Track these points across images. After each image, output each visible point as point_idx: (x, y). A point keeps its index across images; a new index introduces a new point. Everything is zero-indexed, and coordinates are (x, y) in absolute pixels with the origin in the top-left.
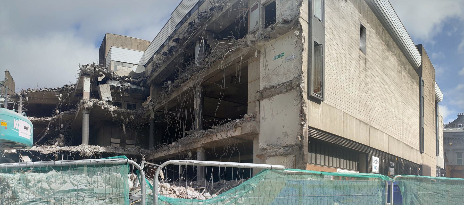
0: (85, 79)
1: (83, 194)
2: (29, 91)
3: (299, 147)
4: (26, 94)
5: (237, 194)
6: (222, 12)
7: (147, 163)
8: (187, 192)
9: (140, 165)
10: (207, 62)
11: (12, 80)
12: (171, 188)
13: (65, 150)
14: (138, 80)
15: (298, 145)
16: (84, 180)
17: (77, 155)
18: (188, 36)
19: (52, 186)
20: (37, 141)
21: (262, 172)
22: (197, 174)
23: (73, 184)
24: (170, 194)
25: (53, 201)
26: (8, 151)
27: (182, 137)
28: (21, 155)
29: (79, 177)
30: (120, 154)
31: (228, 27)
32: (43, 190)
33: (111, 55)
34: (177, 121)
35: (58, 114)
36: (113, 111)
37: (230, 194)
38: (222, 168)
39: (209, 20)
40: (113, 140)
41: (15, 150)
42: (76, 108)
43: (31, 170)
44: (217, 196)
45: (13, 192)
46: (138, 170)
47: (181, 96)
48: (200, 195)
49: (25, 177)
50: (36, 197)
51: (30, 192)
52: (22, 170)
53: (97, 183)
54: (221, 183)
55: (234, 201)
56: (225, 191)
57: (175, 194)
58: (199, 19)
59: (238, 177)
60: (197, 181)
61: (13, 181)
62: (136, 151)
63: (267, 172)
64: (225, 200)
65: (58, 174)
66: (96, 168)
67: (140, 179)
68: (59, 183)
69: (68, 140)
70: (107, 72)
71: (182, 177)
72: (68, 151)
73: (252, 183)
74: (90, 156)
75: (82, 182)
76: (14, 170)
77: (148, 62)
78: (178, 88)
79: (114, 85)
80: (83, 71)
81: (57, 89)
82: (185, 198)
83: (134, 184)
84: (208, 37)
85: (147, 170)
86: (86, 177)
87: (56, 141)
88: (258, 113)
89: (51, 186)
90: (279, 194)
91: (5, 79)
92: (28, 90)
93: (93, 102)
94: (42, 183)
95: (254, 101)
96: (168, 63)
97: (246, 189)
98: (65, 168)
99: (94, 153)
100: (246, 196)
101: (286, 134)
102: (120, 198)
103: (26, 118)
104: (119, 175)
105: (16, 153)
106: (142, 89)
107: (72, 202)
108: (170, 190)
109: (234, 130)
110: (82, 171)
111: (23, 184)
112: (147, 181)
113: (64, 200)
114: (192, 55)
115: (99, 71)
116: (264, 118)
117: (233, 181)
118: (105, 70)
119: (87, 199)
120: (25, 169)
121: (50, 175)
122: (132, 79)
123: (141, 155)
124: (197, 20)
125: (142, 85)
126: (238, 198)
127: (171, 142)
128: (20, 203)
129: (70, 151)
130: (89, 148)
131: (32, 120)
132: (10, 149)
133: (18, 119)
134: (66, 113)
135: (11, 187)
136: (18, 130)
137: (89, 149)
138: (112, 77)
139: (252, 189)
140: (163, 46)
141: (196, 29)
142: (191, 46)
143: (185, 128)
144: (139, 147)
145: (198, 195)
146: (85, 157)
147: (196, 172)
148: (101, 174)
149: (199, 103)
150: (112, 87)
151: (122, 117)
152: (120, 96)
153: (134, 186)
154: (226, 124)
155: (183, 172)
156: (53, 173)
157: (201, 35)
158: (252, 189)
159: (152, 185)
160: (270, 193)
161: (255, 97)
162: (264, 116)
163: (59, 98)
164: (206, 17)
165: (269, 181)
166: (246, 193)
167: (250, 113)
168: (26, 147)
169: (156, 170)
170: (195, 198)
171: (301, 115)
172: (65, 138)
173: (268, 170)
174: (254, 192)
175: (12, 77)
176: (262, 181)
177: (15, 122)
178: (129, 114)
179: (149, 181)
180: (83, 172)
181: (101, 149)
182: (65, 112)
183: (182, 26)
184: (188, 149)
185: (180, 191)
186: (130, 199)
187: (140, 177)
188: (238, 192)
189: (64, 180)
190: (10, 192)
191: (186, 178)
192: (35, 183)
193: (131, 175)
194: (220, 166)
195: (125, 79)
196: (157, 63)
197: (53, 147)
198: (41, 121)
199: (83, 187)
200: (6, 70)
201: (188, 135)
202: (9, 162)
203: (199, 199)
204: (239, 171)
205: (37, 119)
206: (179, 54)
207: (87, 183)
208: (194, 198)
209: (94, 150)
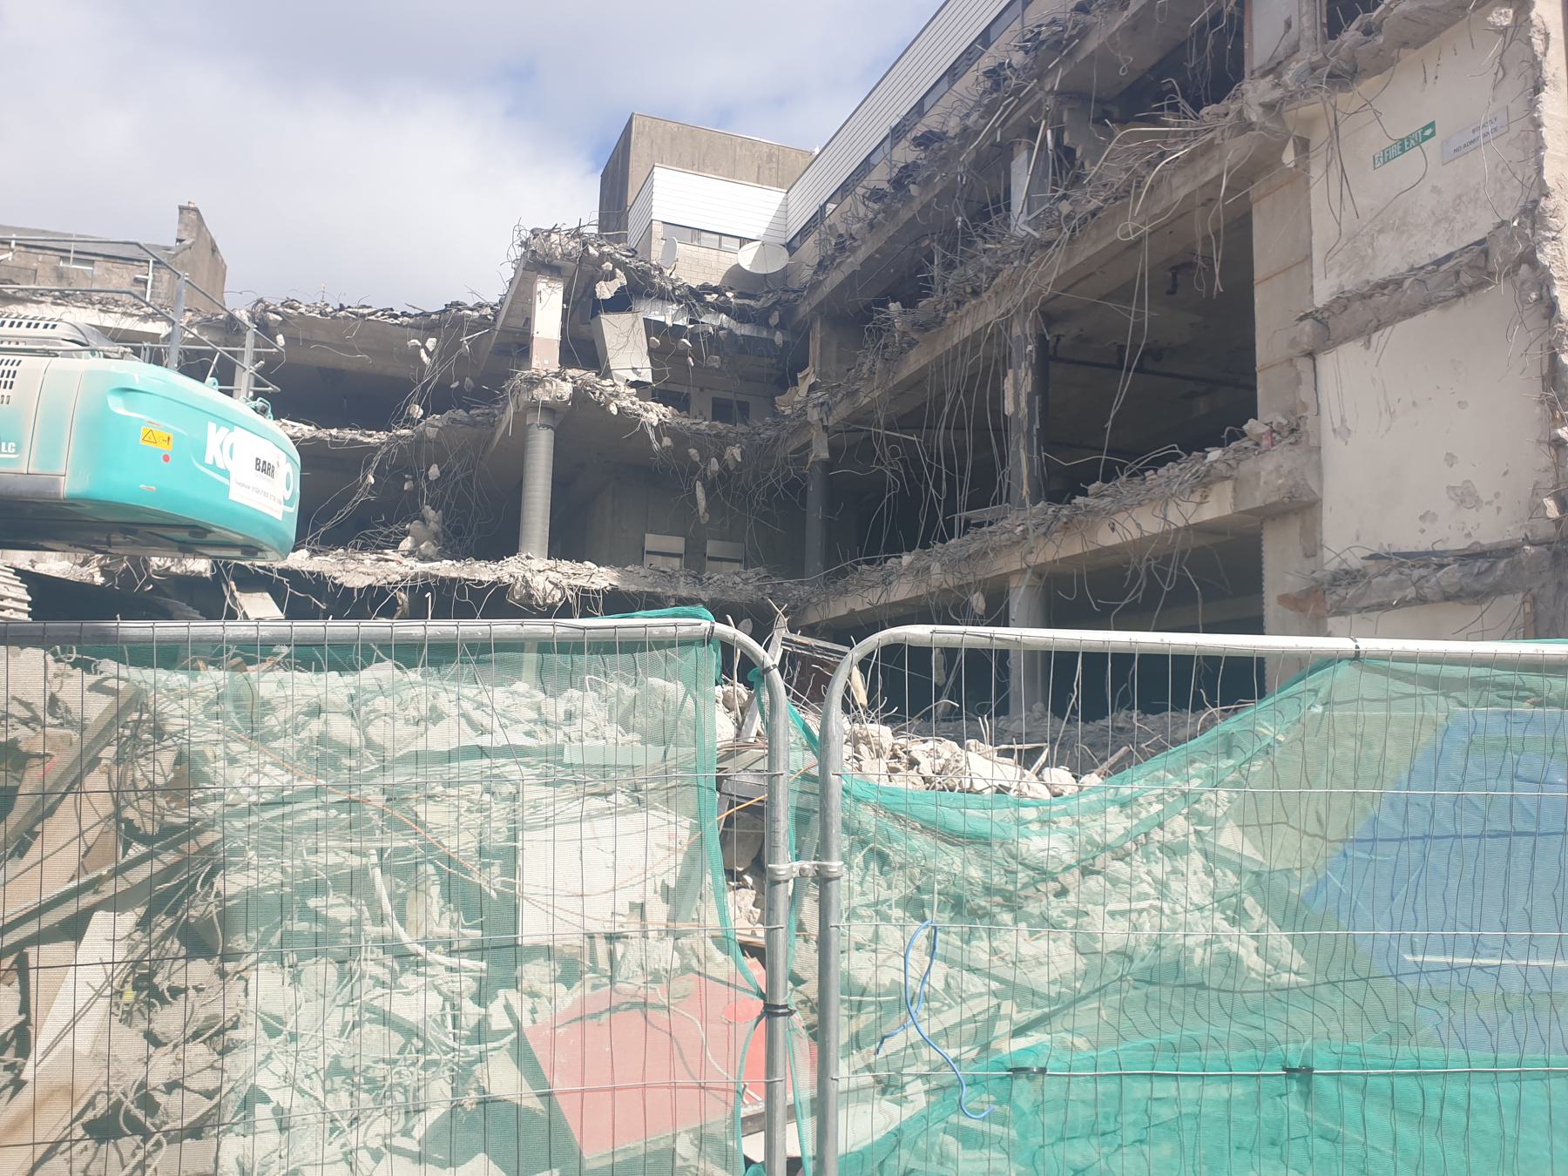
0: (542, 285)
1: (517, 768)
2: (290, 311)
3: (1550, 554)
4: (276, 320)
5: (1193, 777)
6: (1126, 13)
7: (795, 637)
8: (967, 762)
9: (766, 649)
10: (1069, 217)
11: (214, 250)
12: (897, 747)
13: (441, 574)
14: (760, 303)
15: (1547, 543)
16: (524, 710)
17: (498, 602)
18: (982, 122)
19: (377, 732)
20: (316, 528)
21: (1311, 672)
22: (1012, 685)
23: (472, 724)
24: (895, 770)
25: (378, 800)
26: (168, 564)
27: (951, 537)
28: (234, 588)
29: (500, 695)
30: (681, 601)
31: (1152, 69)
32: (329, 751)
33: (652, 186)
34: (930, 467)
35: (419, 422)
36: (655, 424)
37: (1162, 772)
38: (1123, 659)
39: (1070, 54)
40: (652, 541)
41: (204, 561)
42: (496, 402)
43: (279, 658)
44: (1100, 780)
45: (179, 760)
46: (758, 669)
47: (947, 364)
48: (1023, 775)
49: (245, 691)
50: (295, 783)
51: (268, 759)
52: (235, 655)
53: (578, 721)
54: (1120, 725)
55: (1180, 805)
56: (1139, 762)
57: (913, 772)
58: (1027, 53)
59: (1197, 695)
60: (1011, 712)
61: (187, 707)
62: (750, 587)
63: (1338, 675)
64: (1141, 800)
65: (406, 680)
66: (576, 657)
67: (766, 708)
68: (407, 721)
69: (457, 532)
70: (633, 263)
71: (944, 701)
72: (455, 579)
73: (1265, 724)
74: (553, 606)
75: (516, 715)
76: (193, 654)
77: (804, 232)
78: (934, 330)
79: (661, 319)
80: (534, 252)
81: (416, 315)
82: (958, 788)
83: (739, 728)
84: (1065, 118)
85: (794, 669)
86: (532, 696)
87: (406, 534)
88: (1313, 410)
89: (371, 730)
90: (1404, 776)
91: (179, 241)
92: (289, 304)
93: (575, 382)
94: (330, 716)
95: (1290, 360)
96: (890, 229)
97: (1237, 752)
98: (441, 654)
99: (569, 592)
100: (1236, 784)
101: (1465, 497)
102: (679, 790)
103: (269, 423)
104: (675, 689)
105: (208, 574)
106: (779, 338)
107: (465, 804)
108: (895, 756)
109: (1197, 497)
110: (516, 670)
111: (237, 723)
112: (795, 715)
113: (430, 797)
114: (998, 196)
115: (603, 257)
116: (1343, 432)
117: (1174, 714)
118: (627, 256)
119: (534, 792)
120: (252, 652)
121: (368, 682)
122: (735, 297)
123: (769, 604)
124: (1018, 58)
125: (777, 321)
126: (1201, 794)
127: (895, 549)
128: (210, 813)
129: (466, 580)
130: (550, 573)
131: (299, 435)
132: (181, 555)
133: (229, 422)
134: (454, 421)
135: (172, 735)
136: (225, 473)
137: (552, 575)
138: (653, 285)
139: (1267, 751)
140: (866, 166)
141: (1019, 89)
142: (996, 160)
143: (963, 497)
144: (762, 571)
145: (1018, 779)
146: (529, 608)
147: (1008, 676)
148: (599, 683)
149: (1029, 389)
150: (653, 328)
151: (693, 451)
152: (688, 364)
153: (738, 735)
154: (1156, 471)
155: (948, 678)
156: (382, 672)
157: (1037, 110)
158: (1268, 753)
159: (817, 733)
160: (1356, 771)
161: (1293, 343)
162: (1343, 420)
163: (422, 351)
164: (1059, 42)
165: (1348, 713)
166: (1237, 768)
167: (1268, 413)
168: (262, 551)
169: (833, 670)
170: (1002, 790)
171: (1553, 394)
172: (444, 523)
173: (1339, 661)
174: (1274, 768)
175: (212, 241)
176: (1314, 716)
177: (215, 437)
178: (722, 442)
179: (802, 715)
180: (520, 672)
181: (602, 578)
182: (449, 413)
183: (954, 87)
184: (970, 579)
185: (937, 761)
186: (721, 793)
187: (766, 698)
188: (1201, 767)
189: (433, 709)
190: (167, 759)
191: (961, 704)
192: (294, 717)
193: (727, 688)
194: (1113, 648)
195: (709, 298)
196: (841, 231)
197: (387, 560)
198: (341, 444)
199: (518, 739)
200: (186, 205)
201: (980, 525)
202: (167, 615)
203: (1021, 794)
204: (1198, 672)
205: (322, 434)
206: (937, 191)
207: (535, 722)
208: (998, 791)
209: (573, 582)
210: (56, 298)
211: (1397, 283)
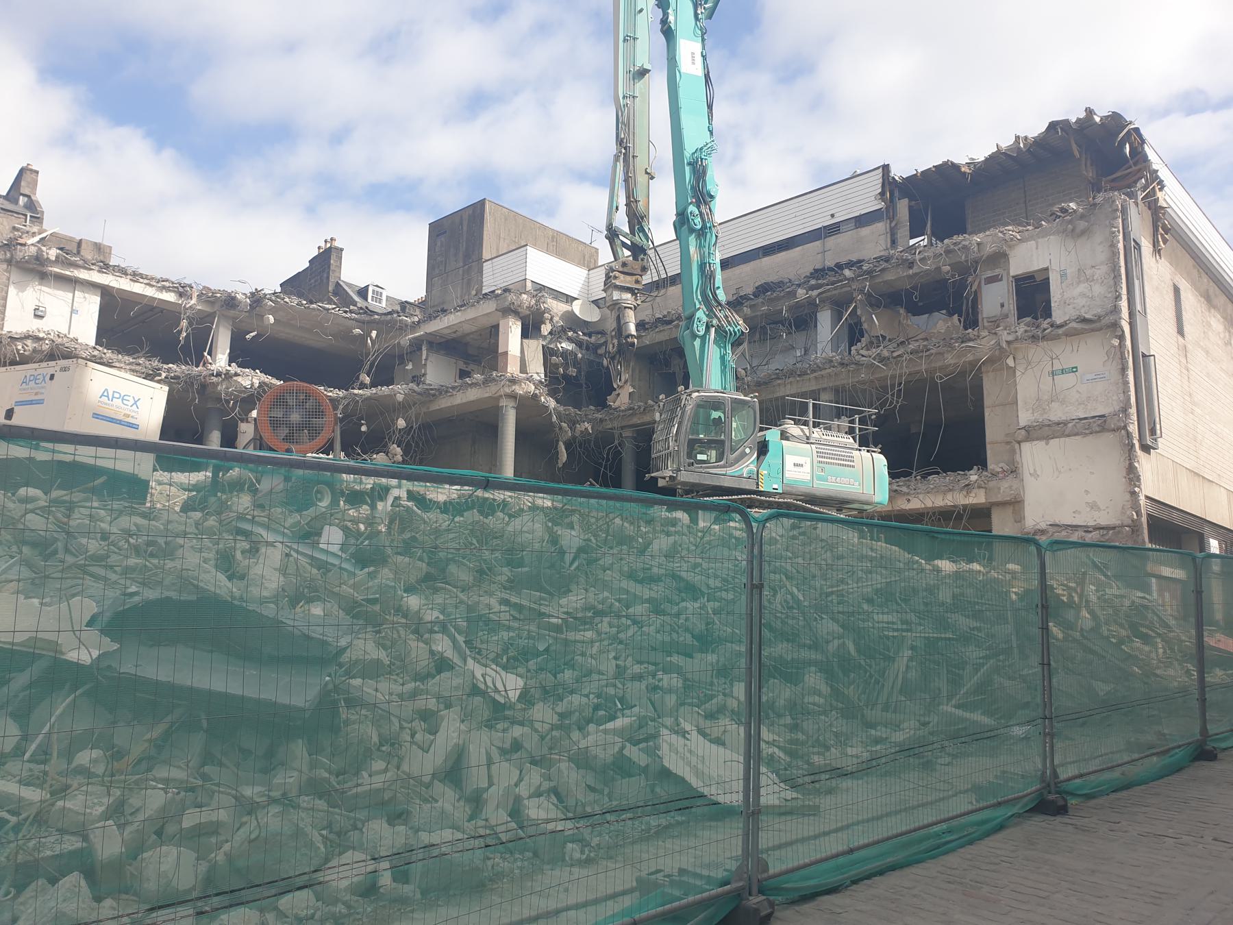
101: (1094, 506)
210: (101, 267)
211: (1065, 423)
